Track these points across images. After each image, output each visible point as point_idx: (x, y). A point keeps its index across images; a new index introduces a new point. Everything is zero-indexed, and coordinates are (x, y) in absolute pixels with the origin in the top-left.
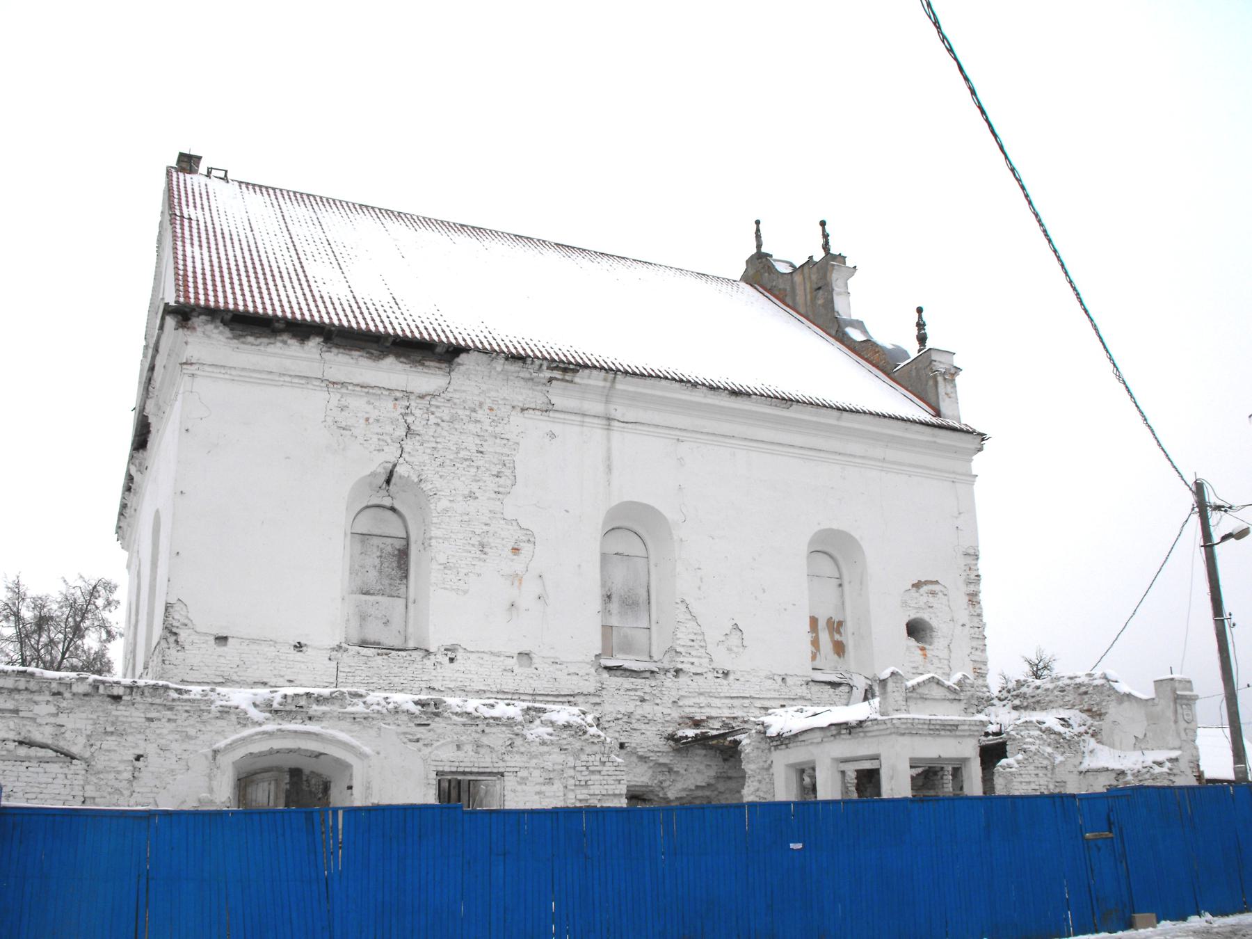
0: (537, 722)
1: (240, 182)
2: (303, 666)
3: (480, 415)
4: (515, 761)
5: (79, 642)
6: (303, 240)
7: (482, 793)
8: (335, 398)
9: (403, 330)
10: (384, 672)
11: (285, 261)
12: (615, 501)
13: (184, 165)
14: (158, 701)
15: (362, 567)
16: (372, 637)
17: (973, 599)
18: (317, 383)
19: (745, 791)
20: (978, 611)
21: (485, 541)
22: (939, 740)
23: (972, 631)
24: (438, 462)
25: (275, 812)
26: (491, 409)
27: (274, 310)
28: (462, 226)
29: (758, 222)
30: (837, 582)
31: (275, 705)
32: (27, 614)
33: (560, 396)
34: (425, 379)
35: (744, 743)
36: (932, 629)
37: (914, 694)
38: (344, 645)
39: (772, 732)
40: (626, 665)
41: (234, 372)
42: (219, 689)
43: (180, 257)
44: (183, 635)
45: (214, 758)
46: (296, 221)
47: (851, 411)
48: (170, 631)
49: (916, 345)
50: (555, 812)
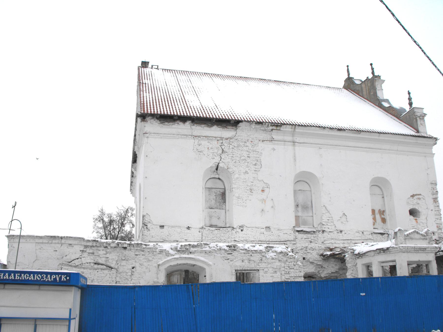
0: (271, 251)
1: (163, 69)
2: (190, 235)
3: (248, 144)
4: (263, 265)
5: (123, 228)
6: (184, 87)
7: (251, 277)
8: (197, 141)
9: (219, 116)
10: (218, 236)
11: (178, 95)
12: (298, 172)
13: (143, 65)
14: (139, 249)
15: (209, 199)
16: (214, 223)
17: (435, 200)
18: (190, 137)
19: (347, 274)
20: (438, 205)
21: (252, 188)
22: (418, 254)
23: (436, 212)
24: (234, 161)
25: (181, 285)
26: (252, 142)
27: (174, 113)
28: (240, 77)
29: (348, 66)
30: (381, 196)
31: (178, 249)
32: (106, 220)
33: (276, 135)
34: (227, 133)
35: (346, 256)
36: (419, 212)
37: (408, 237)
38: (204, 227)
39: (356, 252)
40: (304, 229)
41: (161, 135)
42: (159, 244)
43: (142, 97)
44: (149, 226)
45: (158, 267)
46: (182, 81)
47: (384, 133)
48: (145, 225)
49: (409, 107)
50: (274, 284)
